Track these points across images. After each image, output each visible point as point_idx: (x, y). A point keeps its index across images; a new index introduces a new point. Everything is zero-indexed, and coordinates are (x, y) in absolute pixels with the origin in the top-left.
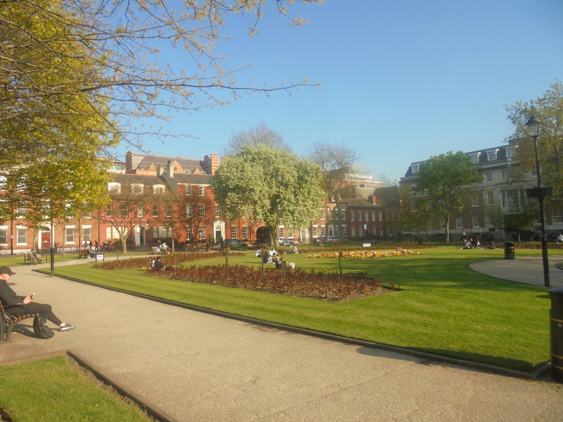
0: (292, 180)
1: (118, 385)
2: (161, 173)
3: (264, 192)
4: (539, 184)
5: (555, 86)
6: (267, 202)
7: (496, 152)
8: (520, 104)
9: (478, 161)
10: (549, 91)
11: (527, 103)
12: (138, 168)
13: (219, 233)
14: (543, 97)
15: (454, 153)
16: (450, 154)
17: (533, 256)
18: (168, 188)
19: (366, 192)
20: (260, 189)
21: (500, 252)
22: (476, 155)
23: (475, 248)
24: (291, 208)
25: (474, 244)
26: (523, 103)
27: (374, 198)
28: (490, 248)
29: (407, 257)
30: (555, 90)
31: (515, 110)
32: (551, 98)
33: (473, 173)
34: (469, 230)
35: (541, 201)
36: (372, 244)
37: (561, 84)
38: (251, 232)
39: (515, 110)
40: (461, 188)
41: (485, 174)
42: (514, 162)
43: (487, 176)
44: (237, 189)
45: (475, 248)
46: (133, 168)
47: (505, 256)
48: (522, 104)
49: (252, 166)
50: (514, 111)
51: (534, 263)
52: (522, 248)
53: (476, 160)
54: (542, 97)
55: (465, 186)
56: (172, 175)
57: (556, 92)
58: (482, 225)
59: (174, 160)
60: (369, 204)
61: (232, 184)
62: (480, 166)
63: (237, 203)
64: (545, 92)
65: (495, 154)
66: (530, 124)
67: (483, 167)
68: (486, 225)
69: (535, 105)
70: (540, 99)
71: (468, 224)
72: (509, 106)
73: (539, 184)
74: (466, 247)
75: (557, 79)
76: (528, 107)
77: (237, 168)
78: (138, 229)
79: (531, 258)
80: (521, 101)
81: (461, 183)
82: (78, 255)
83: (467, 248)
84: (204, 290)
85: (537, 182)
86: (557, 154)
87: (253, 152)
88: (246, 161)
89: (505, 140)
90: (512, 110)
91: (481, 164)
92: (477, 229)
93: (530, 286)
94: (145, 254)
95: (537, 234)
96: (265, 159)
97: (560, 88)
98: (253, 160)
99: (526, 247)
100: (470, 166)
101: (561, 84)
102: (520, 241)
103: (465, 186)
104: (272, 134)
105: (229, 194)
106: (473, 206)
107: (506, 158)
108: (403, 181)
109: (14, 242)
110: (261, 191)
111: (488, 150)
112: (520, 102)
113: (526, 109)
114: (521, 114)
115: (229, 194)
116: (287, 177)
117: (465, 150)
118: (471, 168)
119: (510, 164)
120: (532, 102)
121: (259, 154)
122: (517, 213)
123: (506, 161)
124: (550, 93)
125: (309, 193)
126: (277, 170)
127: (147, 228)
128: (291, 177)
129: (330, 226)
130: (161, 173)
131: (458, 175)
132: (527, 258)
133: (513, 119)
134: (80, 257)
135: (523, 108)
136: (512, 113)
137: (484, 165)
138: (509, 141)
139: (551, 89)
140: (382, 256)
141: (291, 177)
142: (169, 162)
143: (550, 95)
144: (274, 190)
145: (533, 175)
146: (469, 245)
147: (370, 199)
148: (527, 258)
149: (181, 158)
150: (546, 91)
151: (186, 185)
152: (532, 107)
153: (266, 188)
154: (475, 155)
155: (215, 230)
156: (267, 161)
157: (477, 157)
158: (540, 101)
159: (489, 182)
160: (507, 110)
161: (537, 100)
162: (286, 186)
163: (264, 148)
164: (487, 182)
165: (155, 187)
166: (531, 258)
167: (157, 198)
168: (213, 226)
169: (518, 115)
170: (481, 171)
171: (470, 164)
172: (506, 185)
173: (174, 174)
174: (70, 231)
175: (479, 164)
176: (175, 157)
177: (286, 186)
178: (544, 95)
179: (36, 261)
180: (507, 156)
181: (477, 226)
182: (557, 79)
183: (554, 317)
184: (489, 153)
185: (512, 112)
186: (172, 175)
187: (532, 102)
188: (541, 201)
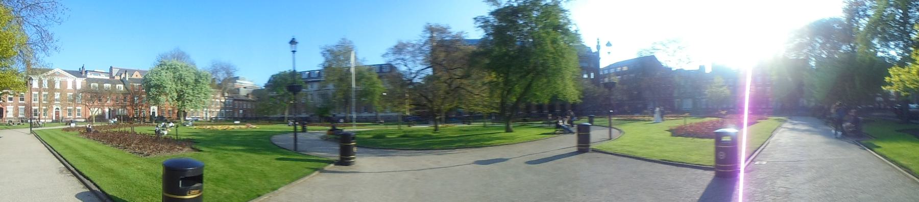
0: (191, 81)
1: (373, 154)
2: (122, 78)
3: (172, 88)
6: (175, 95)
12: (116, 75)
13: (154, 113)
18: (125, 87)
19: (243, 92)
20: (170, 86)
21: (570, 141)
24: (190, 98)
27: (250, 95)
29: (249, 129)
36: (241, 122)
38: (174, 113)
44: (157, 86)
46: (113, 76)
49: (166, 73)
56: (127, 79)
59: (135, 71)
60: (246, 98)
61: (153, 83)
63: (156, 95)
77: (157, 74)
78: (107, 110)
82: (65, 124)
84: (86, 146)
87: (168, 64)
88: (163, 69)
96: (174, 68)
98: (168, 68)
104: (183, 54)
105: (151, 89)
108: (266, 86)
109: (41, 116)
110: (170, 88)
115: (151, 89)
116: (188, 79)
121: (171, 65)
125: (201, 89)
126: (181, 75)
127: (112, 109)
128: (190, 80)
129: (222, 111)
130: (122, 78)
134: (66, 125)
140: (233, 129)
141: (190, 80)
142: (126, 71)
144: (179, 87)
147: (247, 96)
149: (140, 69)
151: (135, 84)
153: (174, 86)
155: (151, 111)
156: (175, 70)
162: (187, 85)
163: (175, 62)
165: (105, 85)
167: (118, 93)
168: (150, 109)
173: (129, 79)
174: (70, 110)
176: (137, 69)
177: (187, 85)
179: (38, 126)
186: (127, 79)
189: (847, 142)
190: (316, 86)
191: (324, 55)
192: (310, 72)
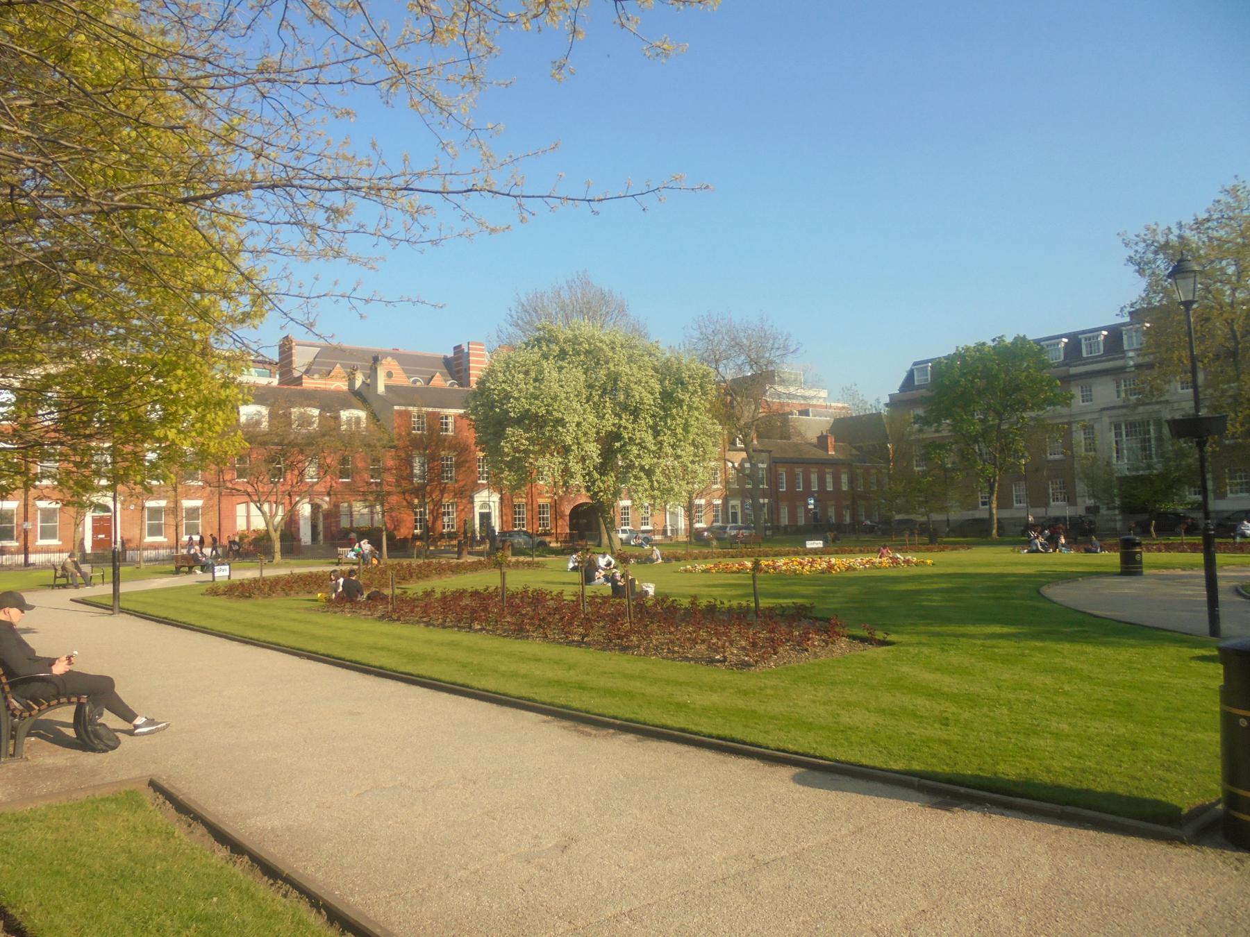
0: (649, 399)
1: (263, 854)
2: (358, 384)
3: (585, 426)
4: (1197, 409)
5: (1233, 192)
6: (593, 449)
7: (1102, 337)
8: (1155, 230)
9: (1062, 358)
10: (1219, 201)
11: (1169, 229)
12: (307, 372)
13: (486, 517)
14: (1206, 216)
15: (1009, 339)
16: (999, 342)
17: (1183, 569)
18: (374, 416)
19: (813, 426)
20: (577, 419)
22: (1058, 344)
23: (1055, 551)
24: (647, 462)
25: (1052, 542)
26: (1162, 228)
27: (831, 441)
28: (1088, 551)
29: (904, 571)
30: (1231, 201)
31: (1143, 245)
32: (1223, 217)
33: (1050, 384)
34: (1041, 512)
35: (1201, 445)
36: (826, 541)
37: (1245, 187)
38: (557, 514)
39: (1143, 245)
40: (1023, 418)
41: (1077, 386)
42: (1140, 360)
43: (1082, 391)
44: (527, 420)
45: (1055, 551)
46: (296, 374)
47: (1122, 568)
48: (1159, 231)
49: (560, 369)
50: (1141, 247)
51: (1185, 584)
52: (1160, 551)
53: (1057, 355)
54: (1203, 215)
55: (1033, 414)
56: (381, 389)
57: (1235, 205)
58: (1071, 500)
59: (386, 355)
60: (818, 454)
61: (514, 408)
62: (1066, 368)
63: (526, 452)
64: (1210, 205)
65: (1098, 343)
66: (1177, 276)
67: (1073, 370)
68: (1079, 500)
69: (1188, 234)
70: (1200, 219)
71: (1038, 498)
72: (1131, 236)
73: (1197, 409)
74: (1034, 548)
75: (1236, 176)
76: (1173, 238)
77: (527, 373)
78: (305, 509)
79: (1179, 572)
80: (1156, 224)
81: (1024, 406)
82: (172, 567)
83: (1037, 551)
84: (452, 644)
85: (1192, 404)
86: (1237, 343)
87: (561, 337)
88: (545, 357)
89: (1122, 310)
90: (1136, 244)
91: (1067, 365)
92: (1059, 509)
93: (1176, 635)
94: (321, 565)
95: (1192, 519)
96: (587, 352)
97: (1243, 195)
98: (563, 354)
99: (1169, 548)
100: (1044, 368)
101: (1245, 187)
102: (1154, 536)
103: (1033, 414)
104: (603, 298)
105: (509, 430)
106: (1051, 457)
107: (1124, 352)
108: (894, 403)
109: (30, 538)
110: (578, 424)
111: (1084, 332)
112: (1155, 227)
113: (1167, 243)
114: (1156, 253)
115: (509, 430)
116: (638, 392)
117: (1033, 334)
118: (1046, 374)
119: (1131, 363)
120: (1180, 226)
121: (574, 341)
122: (1147, 472)
123: (1123, 358)
124: (1221, 207)
125: (686, 428)
126: (614, 378)
127: (325, 506)
128: (646, 394)
129: (733, 502)
130: (358, 384)
131: (1018, 388)
132: (1171, 572)
133: (1139, 264)
134: (177, 572)
135: (1162, 240)
136: (1136, 251)
137: (1075, 366)
138: (1131, 313)
139: (1224, 198)
140: (849, 568)
141: (646, 394)
142: (376, 360)
143: (1221, 211)
144: (609, 423)
145: (1182, 389)
146: (1041, 544)
147: (822, 441)
148: (1171, 572)
149: (402, 350)
150: (1211, 202)
151: (414, 410)
152: (1180, 237)
153: (591, 418)
154: (1054, 345)
155: (477, 511)
156: (593, 357)
157: (1059, 349)
158: (1199, 225)
159: (1086, 404)
160: (1126, 245)
161: (1192, 222)
162: (635, 413)
163: (586, 328)
164: (1081, 404)
165: (345, 414)
166: (1179, 572)
167: (348, 440)
168: (472, 502)
169: (1151, 256)
170: (1067, 379)
171: (1044, 365)
172: (1124, 411)
173: (387, 387)
174: (155, 513)
175: (1065, 364)
176: (388, 348)
177: (635, 413)
178: (1208, 211)
179: (80, 580)
180: (1126, 347)
181: (1060, 503)
182: (1236, 176)
183: (1230, 705)
184: (1086, 339)
185: (1137, 248)
186: (381, 389)
187: (1180, 226)
188: (1201, 445)
189: (1227, 511)
190: (1105, 393)
191: (1141, 266)
192: (1074, 340)
